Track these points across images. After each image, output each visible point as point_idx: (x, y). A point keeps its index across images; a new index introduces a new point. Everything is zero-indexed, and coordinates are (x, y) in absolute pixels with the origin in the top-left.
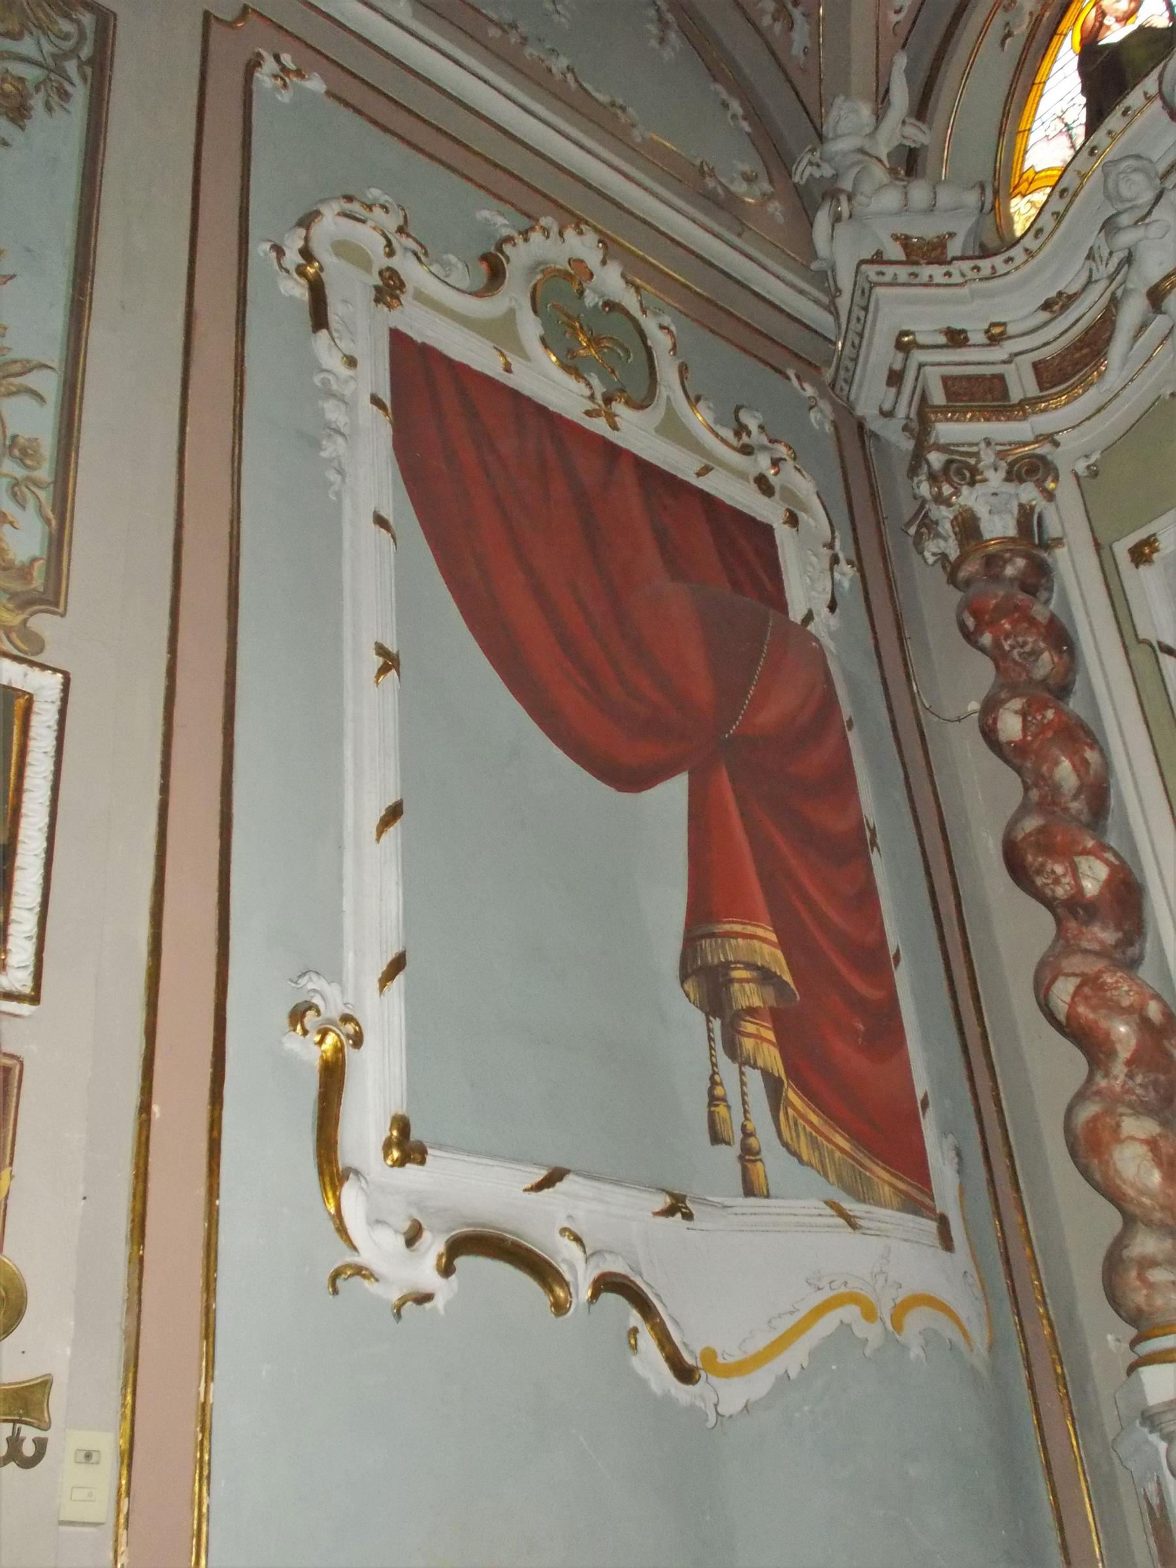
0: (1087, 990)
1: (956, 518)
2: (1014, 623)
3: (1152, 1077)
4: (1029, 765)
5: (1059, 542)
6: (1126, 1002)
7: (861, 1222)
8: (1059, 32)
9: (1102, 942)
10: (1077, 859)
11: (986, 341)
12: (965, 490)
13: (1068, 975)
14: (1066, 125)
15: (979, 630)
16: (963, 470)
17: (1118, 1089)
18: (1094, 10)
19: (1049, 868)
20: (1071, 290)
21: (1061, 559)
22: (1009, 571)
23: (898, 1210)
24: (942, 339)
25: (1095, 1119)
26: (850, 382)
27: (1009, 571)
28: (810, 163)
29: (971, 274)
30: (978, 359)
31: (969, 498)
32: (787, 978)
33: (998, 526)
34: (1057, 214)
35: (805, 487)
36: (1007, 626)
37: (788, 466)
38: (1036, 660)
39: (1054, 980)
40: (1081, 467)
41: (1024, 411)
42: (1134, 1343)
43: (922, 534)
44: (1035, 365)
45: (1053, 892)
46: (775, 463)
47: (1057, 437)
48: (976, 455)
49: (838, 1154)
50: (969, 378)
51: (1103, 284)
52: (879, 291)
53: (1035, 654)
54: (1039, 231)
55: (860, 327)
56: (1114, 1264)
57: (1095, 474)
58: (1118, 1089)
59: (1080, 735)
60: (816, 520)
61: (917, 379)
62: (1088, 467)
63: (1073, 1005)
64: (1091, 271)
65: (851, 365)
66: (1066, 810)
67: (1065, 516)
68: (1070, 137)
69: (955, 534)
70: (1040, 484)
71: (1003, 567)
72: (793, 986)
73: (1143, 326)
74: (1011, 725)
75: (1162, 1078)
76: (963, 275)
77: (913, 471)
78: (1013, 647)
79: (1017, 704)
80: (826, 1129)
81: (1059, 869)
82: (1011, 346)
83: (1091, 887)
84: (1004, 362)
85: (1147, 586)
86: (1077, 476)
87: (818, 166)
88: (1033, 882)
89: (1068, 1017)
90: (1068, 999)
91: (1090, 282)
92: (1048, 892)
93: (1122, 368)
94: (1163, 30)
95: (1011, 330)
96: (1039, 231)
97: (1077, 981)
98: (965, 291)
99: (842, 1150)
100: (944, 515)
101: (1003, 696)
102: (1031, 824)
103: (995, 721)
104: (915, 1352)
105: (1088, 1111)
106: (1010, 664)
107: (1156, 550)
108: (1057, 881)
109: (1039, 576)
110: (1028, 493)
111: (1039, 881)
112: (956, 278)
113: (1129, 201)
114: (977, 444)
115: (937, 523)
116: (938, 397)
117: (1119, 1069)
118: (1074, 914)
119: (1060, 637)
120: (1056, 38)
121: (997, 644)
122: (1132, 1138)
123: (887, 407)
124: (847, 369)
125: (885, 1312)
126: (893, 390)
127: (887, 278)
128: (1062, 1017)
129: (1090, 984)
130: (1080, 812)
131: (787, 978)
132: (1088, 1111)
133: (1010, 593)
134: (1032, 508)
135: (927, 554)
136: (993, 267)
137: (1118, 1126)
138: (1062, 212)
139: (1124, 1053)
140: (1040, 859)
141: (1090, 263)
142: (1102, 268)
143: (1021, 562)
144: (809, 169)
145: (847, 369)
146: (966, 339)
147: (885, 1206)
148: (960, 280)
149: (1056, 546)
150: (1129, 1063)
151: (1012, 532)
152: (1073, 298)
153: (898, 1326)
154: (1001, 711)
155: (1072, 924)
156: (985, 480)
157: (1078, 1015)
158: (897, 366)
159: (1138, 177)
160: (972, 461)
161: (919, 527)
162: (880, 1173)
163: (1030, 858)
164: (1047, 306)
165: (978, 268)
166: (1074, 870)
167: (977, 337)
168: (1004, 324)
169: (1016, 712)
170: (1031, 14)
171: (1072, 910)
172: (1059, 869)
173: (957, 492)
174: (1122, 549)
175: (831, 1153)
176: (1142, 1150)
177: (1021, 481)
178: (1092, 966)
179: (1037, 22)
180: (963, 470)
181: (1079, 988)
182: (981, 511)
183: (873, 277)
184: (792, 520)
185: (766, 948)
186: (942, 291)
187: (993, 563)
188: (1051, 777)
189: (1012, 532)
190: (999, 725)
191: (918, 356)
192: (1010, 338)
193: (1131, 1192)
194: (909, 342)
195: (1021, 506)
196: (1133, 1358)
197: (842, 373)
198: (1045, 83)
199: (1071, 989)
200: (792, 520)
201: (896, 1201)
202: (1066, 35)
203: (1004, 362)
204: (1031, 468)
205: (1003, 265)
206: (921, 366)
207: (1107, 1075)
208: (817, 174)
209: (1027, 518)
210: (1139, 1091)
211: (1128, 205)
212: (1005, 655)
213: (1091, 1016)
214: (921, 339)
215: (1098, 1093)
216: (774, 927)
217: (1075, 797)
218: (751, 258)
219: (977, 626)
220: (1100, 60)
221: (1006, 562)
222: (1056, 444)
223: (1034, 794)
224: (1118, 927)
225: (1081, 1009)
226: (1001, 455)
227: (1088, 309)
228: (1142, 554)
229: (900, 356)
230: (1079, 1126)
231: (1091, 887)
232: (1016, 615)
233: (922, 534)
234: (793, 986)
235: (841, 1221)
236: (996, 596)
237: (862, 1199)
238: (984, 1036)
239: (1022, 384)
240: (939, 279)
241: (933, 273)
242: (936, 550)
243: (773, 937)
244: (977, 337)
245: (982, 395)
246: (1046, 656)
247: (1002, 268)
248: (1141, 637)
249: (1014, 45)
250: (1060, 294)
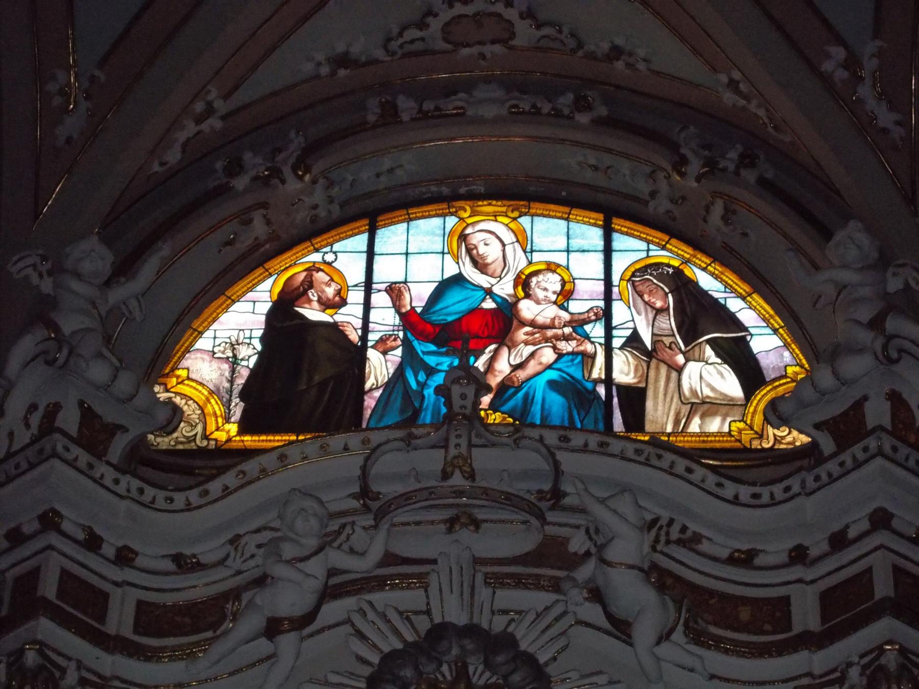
8: (267, 266)
14: (235, 356)
18: (304, 274)
20: (204, 559)
28: (34, 266)
29: (134, 494)
30: (99, 569)
34: (227, 488)
44: (140, 604)
48: (63, 671)
51: (230, 572)
52: (57, 463)
55: (13, 472)
61: (36, 553)
64: (228, 556)
68: (233, 371)
76: (128, 491)
82: (129, 575)
87: (41, 276)
94: (349, 340)
95: (140, 561)
112: (121, 489)
113: (296, 534)
116: (49, 589)
120: (260, 270)
127: (70, 457)
136: (154, 498)
138: (232, 488)
141: (229, 548)
144: (30, 271)
146: (100, 547)
158: (27, 529)
160: (57, 674)
164: (177, 559)
167: (109, 550)
168: (137, 554)
170: (256, 239)
179: (257, 245)
183: (60, 448)
186: (102, 491)
191: (54, 539)
198: (234, 302)
202: (271, 275)
205: (163, 502)
206: (50, 547)
208: (35, 280)
214: (66, 526)
218: (96, 573)
220: (288, 323)
227: (198, 588)
229: (36, 525)
239: (120, 619)
240: (108, 482)
241: (106, 474)
244: (109, 550)
247: (161, 503)
249: (230, 254)
250: (194, 556)
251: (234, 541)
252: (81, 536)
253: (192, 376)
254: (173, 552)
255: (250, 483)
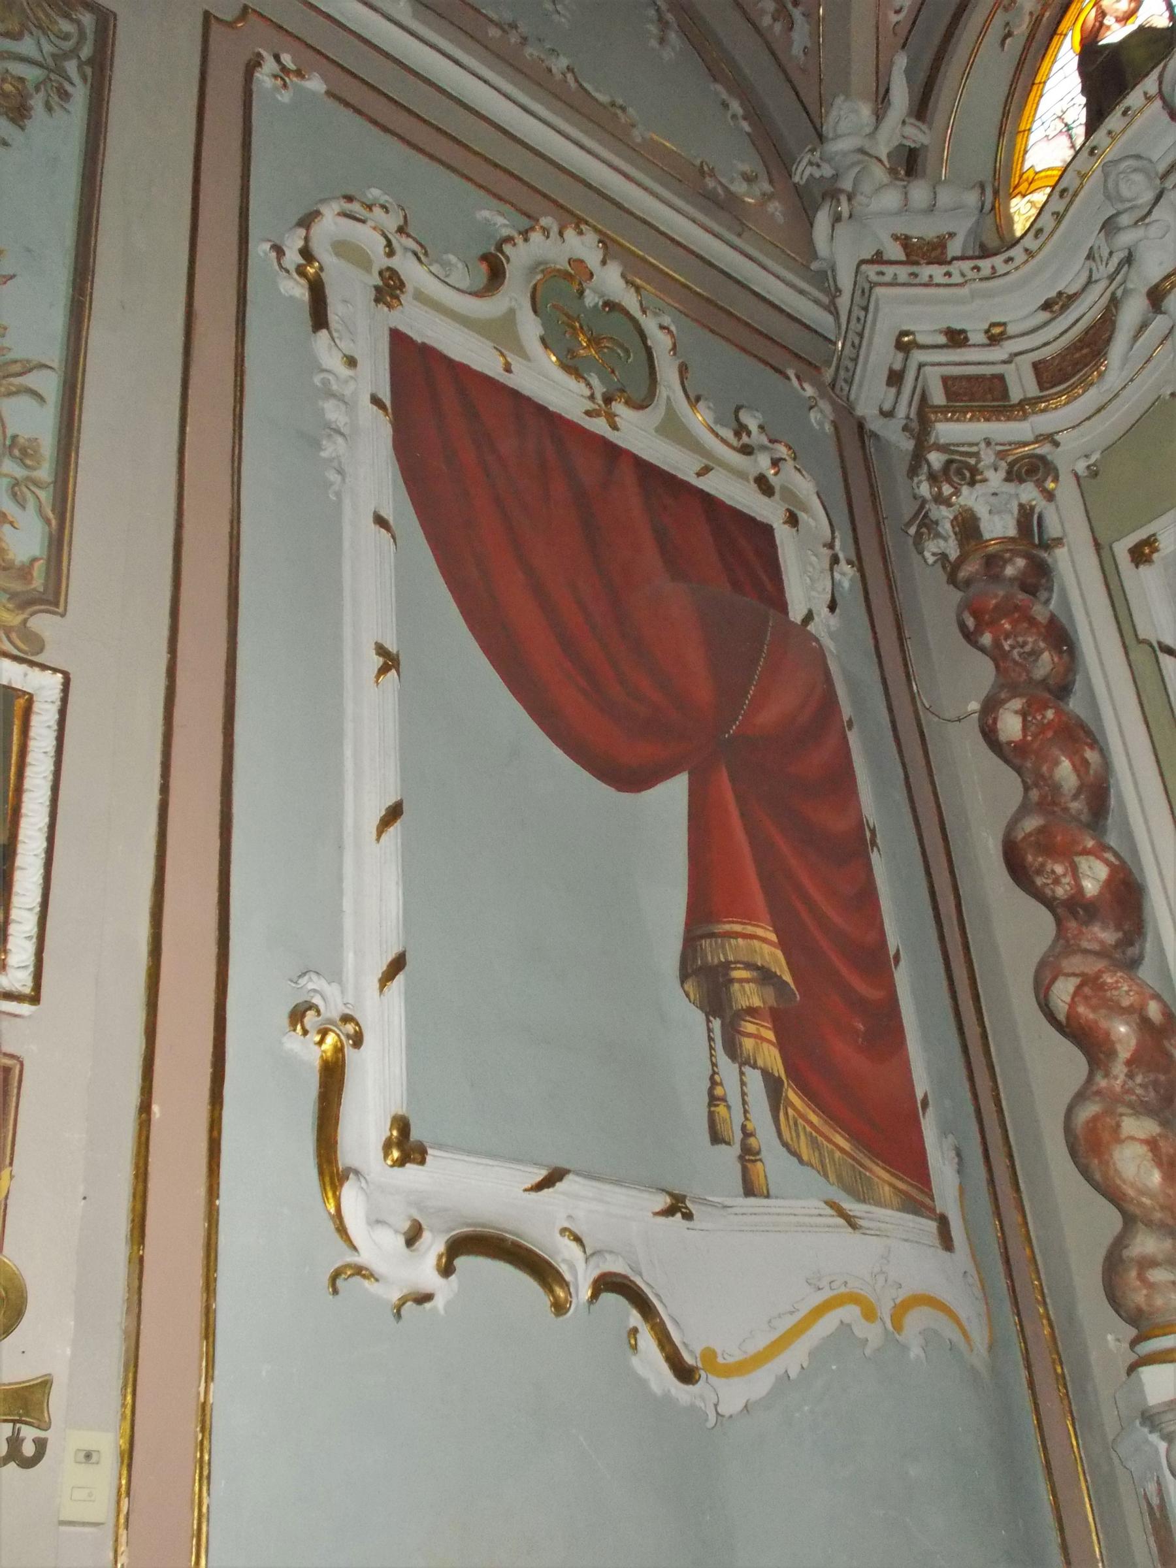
0: (1087, 990)
1: (956, 518)
2: (1014, 623)
3: (1152, 1077)
4: (1029, 765)
5: (1059, 542)
6: (1126, 1002)
7: (861, 1222)
8: (1059, 32)
9: (1102, 942)
10: (1077, 859)
11: (986, 341)
12: (965, 490)
13: (1068, 975)
14: (1066, 125)
15: (979, 630)
16: (963, 470)
17: (1118, 1089)
18: (1094, 10)
19: (1049, 868)
20: (1071, 290)
21: (1061, 559)
22: (1009, 571)
23: (898, 1210)
24: (942, 339)
25: (1095, 1119)
26: (850, 382)
27: (1009, 571)
28: (810, 163)
29: (971, 274)
30: (978, 359)
31: (969, 498)
32: (787, 978)
33: (998, 526)
34: (1057, 214)
35: (805, 487)
36: (1007, 626)
37: (788, 466)
38: (1036, 660)
39: (1054, 980)
40: (1081, 467)
41: (1024, 411)
42: (1134, 1343)
43: (922, 534)
44: (1035, 365)
45: (1053, 892)
46: (775, 463)
47: (1057, 437)
48: (976, 455)
49: (838, 1154)
50: (969, 378)
51: (1103, 284)
52: (879, 291)
53: (1035, 654)
54: (1039, 231)
55: (860, 327)
56: (1114, 1264)
57: (1095, 474)
58: (1118, 1089)
59: (1080, 735)
60: (816, 520)
61: (917, 379)
62: (1088, 467)
63: (1073, 1005)
64: (1091, 271)
65: (851, 365)
66: (1066, 810)
67: (1065, 516)
69: (955, 534)
70: (1040, 484)
71: (1003, 567)
72: (793, 986)
73: (1143, 326)
74: (1011, 725)
75: (1162, 1078)
76: (963, 275)
77: (913, 471)
78: (1013, 647)
79: (1017, 704)
80: (826, 1129)
81: (1059, 869)
82: (1011, 346)
83: (1091, 887)
84: (1004, 362)
85: (1147, 586)
86: (1077, 476)
87: (818, 166)
88: (1033, 882)
89: (1068, 1017)
90: (1068, 999)
91: (1090, 282)
92: (1048, 892)
93: (1122, 368)
94: (1163, 30)
95: (1011, 330)
96: (1039, 231)
97: (1077, 981)
98: (965, 291)
99: (842, 1150)
100: (944, 515)
101: (1003, 696)
102: (1031, 824)
103: (995, 721)
104: (915, 1352)
105: (1088, 1111)
106: (1010, 664)
107: (1156, 550)
108: (1057, 881)
109: (1039, 576)
110: (1028, 493)
111: (1039, 881)
112: (956, 278)
113: (1129, 201)
114: (977, 444)
115: (937, 523)
116: (938, 397)
117: (1119, 1069)
118: (1074, 914)
119: (1060, 637)
120: (1056, 38)
121: (997, 644)
122: (1132, 1138)
123: (887, 407)
124: (847, 369)
125: (885, 1312)
126: (893, 390)
127: (887, 278)
128: (1062, 1017)
129: (1090, 984)
130: (1080, 812)
131: (787, 978)
132: (1088, 1111)
133: (1010, 593)
134: (1032, 508)
135: (927, 554)
136: (993, 267)
137: (1118, 1126)
138: (1062, 212)
139: (1124, 1053)
140: (1040, 859)
141: (1090, 263)
142: (1102, 268)
143: (1021, 562)
144: (809, 169)
145: (847, 369)
146: (966, 339)
147: (885, 1206)
148: (960, 280)
149: (1056, 546)
150: (1129, 1063)
151: (1012, 532)
152: (1073, 298)
153: (898, 1326)
154: (1001, 711)
155: (1072, 924)
156: (985, 480)
157: (1078, 1015)
158: (897, 366)
159: (1138, 177)
160: (972, 461)
161: (919, 527)
162: (880, 1173)
163: (1030, 858)
164: (1047, 306)
165: (978, 268)
166: (1074, 870)
167: (977, 337)
168: (1004, 324)
169: (1016, 712)
170: (1031, 14)
171: (1072, 910)
172: (1059, 869)
173: (957, 492)
174: (1122, 549)
175: (831, 1153)
176: (1142, 1150)
177: (1021, 481)
178: (1092, 966)
180: (963, 470)
181: (1079, 988)
182: (981, 511)
183: (873, 277)
184: (792, 520)
185: (766, 948)
186: (942, 291)
187: (993, 563)
188: (1051, 777)
189: (1012, 532)
190: (999, 725)
191: (918, 356)
192: (1010, 338)
193: (1131, 1192)
194: (909, 342)
195: (1021, 506)
196: (1133, 1358)
197: (842, 373)
198: (1045, 83)
199: (1071, 989)
200: (792, 520)
201: (896, 1201)
202: (1066, 35)
203: (1004, 362)
204: (1031, 468)
205: (1003, 265)
206: (921, 366)
207: (1107, 1075)
208: (817, 174)
209: (1027, 518)
210: (1139, 1091)
211: (1128, 205)
212: (1005, 655)
213: (1091, 1016)
214: (921, 339)
215: (1098, 1093)
216: (774, 927)
217: (1075, 797)
219: (977, 626)
220: (1100, 60)
221: (1006, 562)
222: (1056, 444)
223: (1034, 794)
224: (1118, 927)
225: (1081, 1009)
226: (1001, 455)
227: (1088, 309)
228: (1142, 554)
229: (900, 356)
230: (1079, 1126)
231: (1091, 887)
232: (1016, 615)
233: (922, 534)
234: (793, 986)
235: (841, 1221)
236: (996, 596)
237: (862, 1199)
238: (984, 1036)
239: (1022, 384)
240: (939, 279)
241: (933, 273)
242: (936, 550)
243: (773, 937)
244: (977, 337)
245: (982, 395)
246: (1046, 656)
247: (1002, 268)
248: (1141, 637)
249: (1014, 45)
250: (1060, 294)
251: (1090, 256)
252: (583, 227)
253: (1038, 169)
254: (944, 326)
255: (1075, 195)
